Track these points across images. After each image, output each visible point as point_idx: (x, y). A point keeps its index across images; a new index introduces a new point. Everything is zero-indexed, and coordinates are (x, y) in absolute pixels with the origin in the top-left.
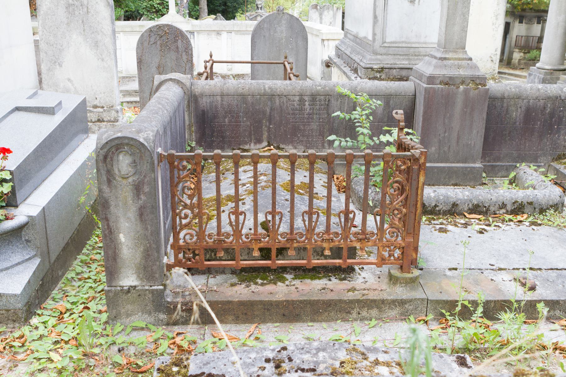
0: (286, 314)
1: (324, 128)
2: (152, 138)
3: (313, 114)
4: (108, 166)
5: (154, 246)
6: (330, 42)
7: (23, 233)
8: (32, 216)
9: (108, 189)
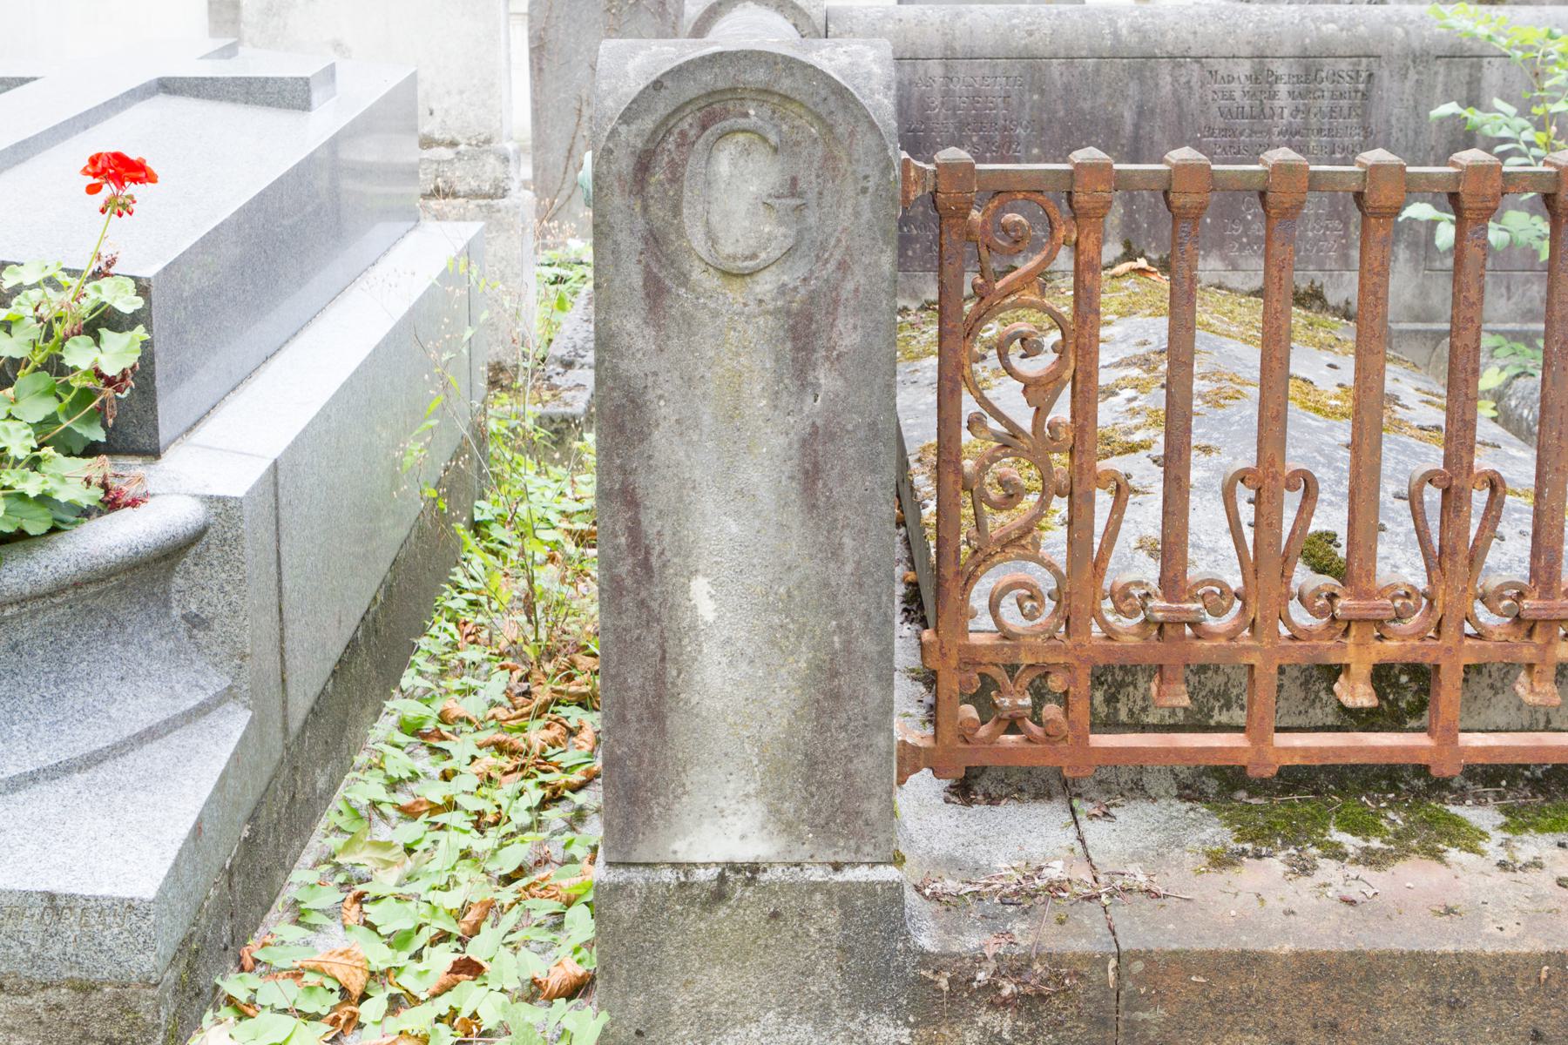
0: (1547, 1031)
2: (876, 69)
4: (656, 210)
5: (868, 646)
7: (178, 581)
8: (222, 500)
9: (650, 332)
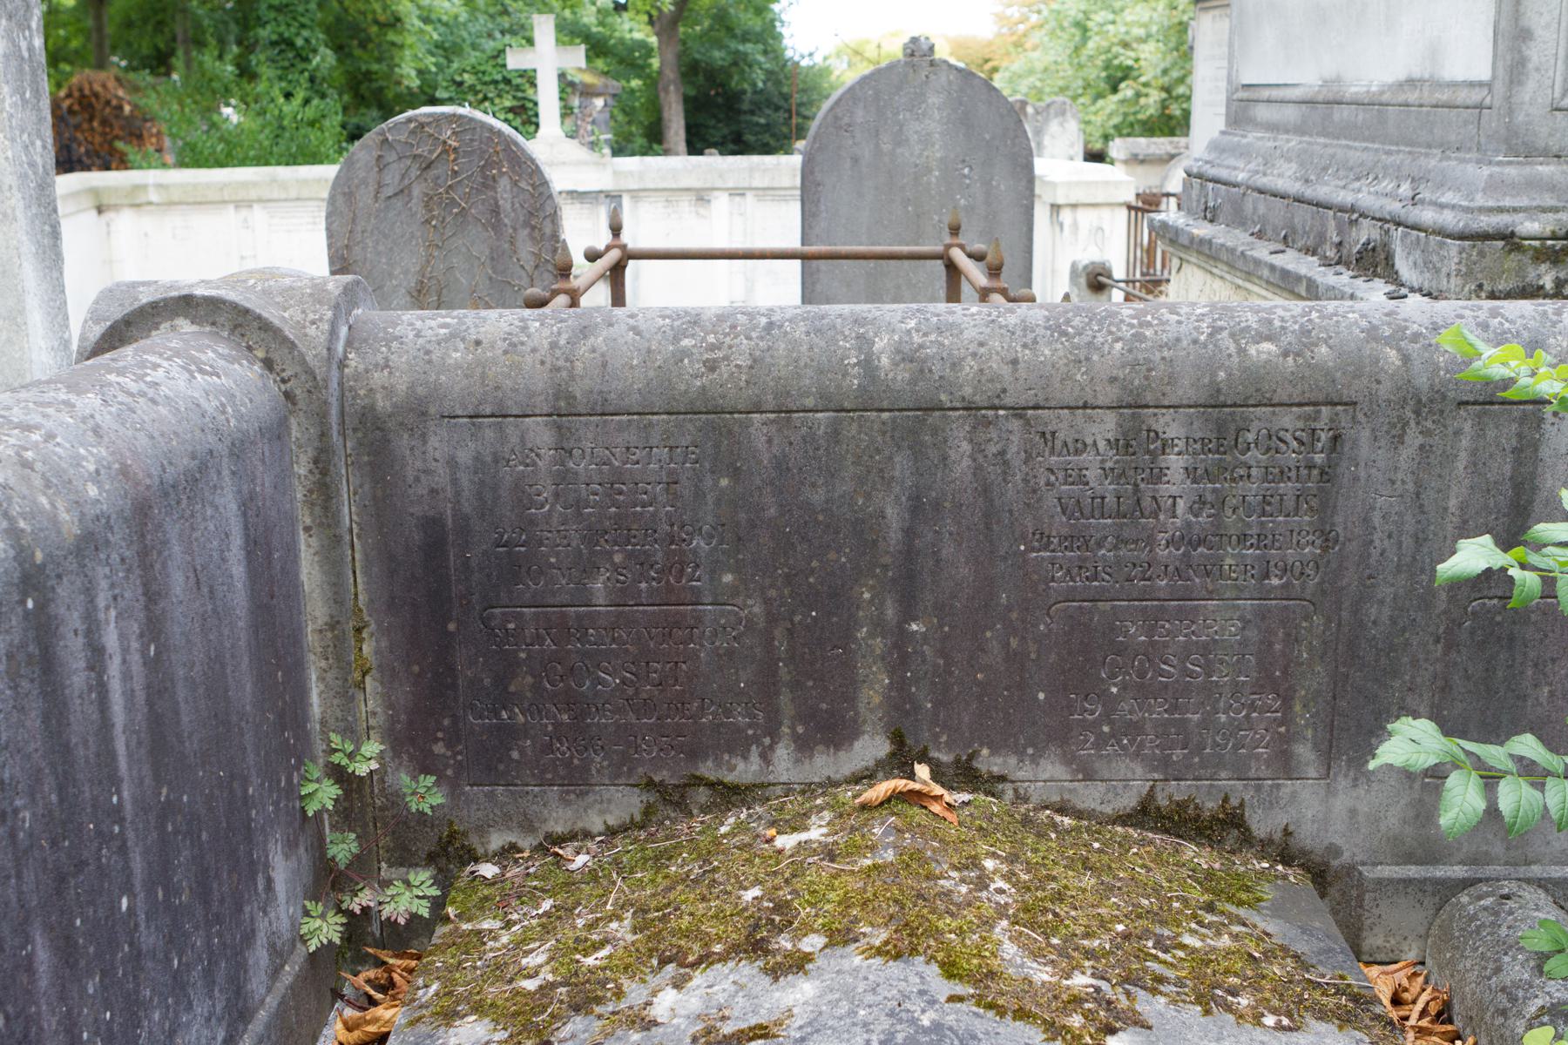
1: (1292, 640)
3: (1214, 537)
6: (1081, 213)
